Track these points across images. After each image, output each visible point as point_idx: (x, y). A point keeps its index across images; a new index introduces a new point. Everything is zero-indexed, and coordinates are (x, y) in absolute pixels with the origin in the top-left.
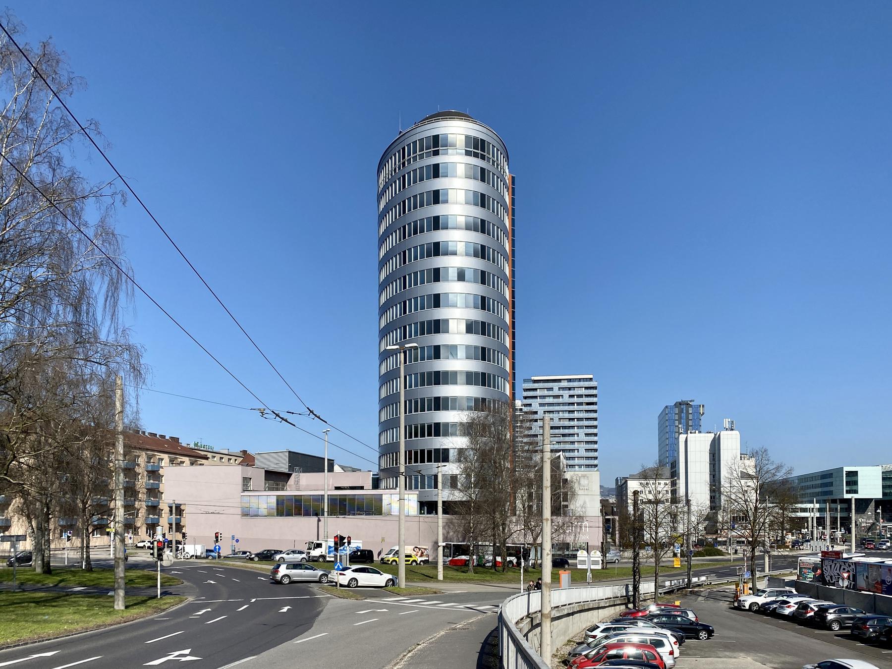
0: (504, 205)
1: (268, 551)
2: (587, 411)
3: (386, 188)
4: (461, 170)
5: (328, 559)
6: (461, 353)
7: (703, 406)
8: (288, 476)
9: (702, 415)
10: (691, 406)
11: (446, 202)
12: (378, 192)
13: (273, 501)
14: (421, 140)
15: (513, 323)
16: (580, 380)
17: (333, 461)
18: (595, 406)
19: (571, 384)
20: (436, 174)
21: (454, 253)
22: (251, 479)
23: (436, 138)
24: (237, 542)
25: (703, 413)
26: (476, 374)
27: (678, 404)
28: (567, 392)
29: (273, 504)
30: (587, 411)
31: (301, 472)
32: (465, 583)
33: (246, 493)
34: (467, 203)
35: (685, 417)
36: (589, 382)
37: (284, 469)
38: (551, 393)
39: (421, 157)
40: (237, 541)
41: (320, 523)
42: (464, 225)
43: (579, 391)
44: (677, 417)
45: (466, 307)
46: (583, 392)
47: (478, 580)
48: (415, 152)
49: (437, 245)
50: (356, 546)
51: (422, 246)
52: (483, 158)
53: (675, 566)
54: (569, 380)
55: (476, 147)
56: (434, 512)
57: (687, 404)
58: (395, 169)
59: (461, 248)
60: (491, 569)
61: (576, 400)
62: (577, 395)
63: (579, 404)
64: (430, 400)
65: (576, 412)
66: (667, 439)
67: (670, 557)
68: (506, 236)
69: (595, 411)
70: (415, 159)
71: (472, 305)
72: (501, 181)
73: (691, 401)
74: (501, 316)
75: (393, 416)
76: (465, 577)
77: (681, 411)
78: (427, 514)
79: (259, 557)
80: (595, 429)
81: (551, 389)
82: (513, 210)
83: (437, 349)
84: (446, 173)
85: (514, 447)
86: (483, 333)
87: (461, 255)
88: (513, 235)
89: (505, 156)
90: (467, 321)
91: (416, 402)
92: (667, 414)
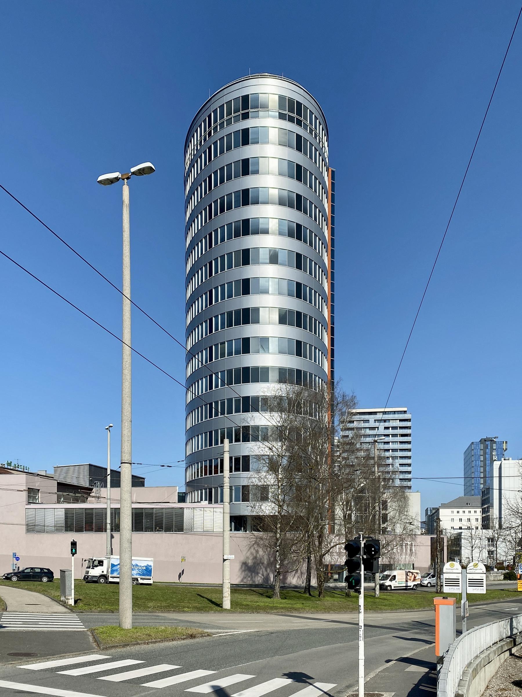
0: (322, 238)
1: (32, 568)
2: (401, 442)
3: (192, 166)
4: (273, 135)
5: (111, 580)
6: (273, 345)
7: (506, 442)
8: (89, 490)
9: (505, 451)
10: (495, 442)
11: (257, 172)
12: (185, 176)
13: (61, 514)
14: (229, 103)
15: (332, 372)
16: (394, 412)
17: (144, 479)
18: (409, 438)
19: (386, 417)
20: (246, 141)
21: (266, 232)
22: (39, 490)
23: (245, 98)
24: (17, 560)
25: (506, 449)
26: (291, 370)
27: (483, 441)
28: (382, 424)
29: (61, 517)
30: (401, 442)
31: (102, 487)
32: (263, 613)
33: (32, 506)
34: (280, 174)
35: (489, 453)
36: (403, 415)
37: (84, 482)
38: (367, 425)
39: (229, 122)
40: (18, 559)
41: (113, 540)
42: (277, 200)
43: (394, 423)
44: (482, 453)
45: (279, 294)
46: (398, 424)
47: (282, 608)
48: (222, 117)
49: (246, 222)
50: (146, 565)
51: (229, 225)
52: (299, 123)
53: (519, 590)
54: (385, 413)
55: (291, 110)
56: (242, 528)
57: (492, 441)
58: (201, 142)
59: (273, 225)
60: (305, 592)
61: (390, 431)
62: (391, 427)
63: (394, 435)
64: (238, 401)
65: (391, 443)
66: (473, 473)
67: (500, 580)
68: (324, 275)
69: (409, 443)
70: (222, 125)
71: (286, 292)
72: (319, 239)
73: (495, 438)
74: (319, 363)
75: (198, 421)
76: (267, 604)
77: (486, 447)
78: (235, 530)
79: (18, 577)
80: (409, 460)
81: (367, 421)
82: (332, 273)
83: (246, 342)
84: (256, 138)
85: (333, 456)
86: (299, 325)
87: (273, 234)
88: (333, 301)
89: (324, 128)
90: (280, 310)
91: (223, 404)
92: (473, 450)
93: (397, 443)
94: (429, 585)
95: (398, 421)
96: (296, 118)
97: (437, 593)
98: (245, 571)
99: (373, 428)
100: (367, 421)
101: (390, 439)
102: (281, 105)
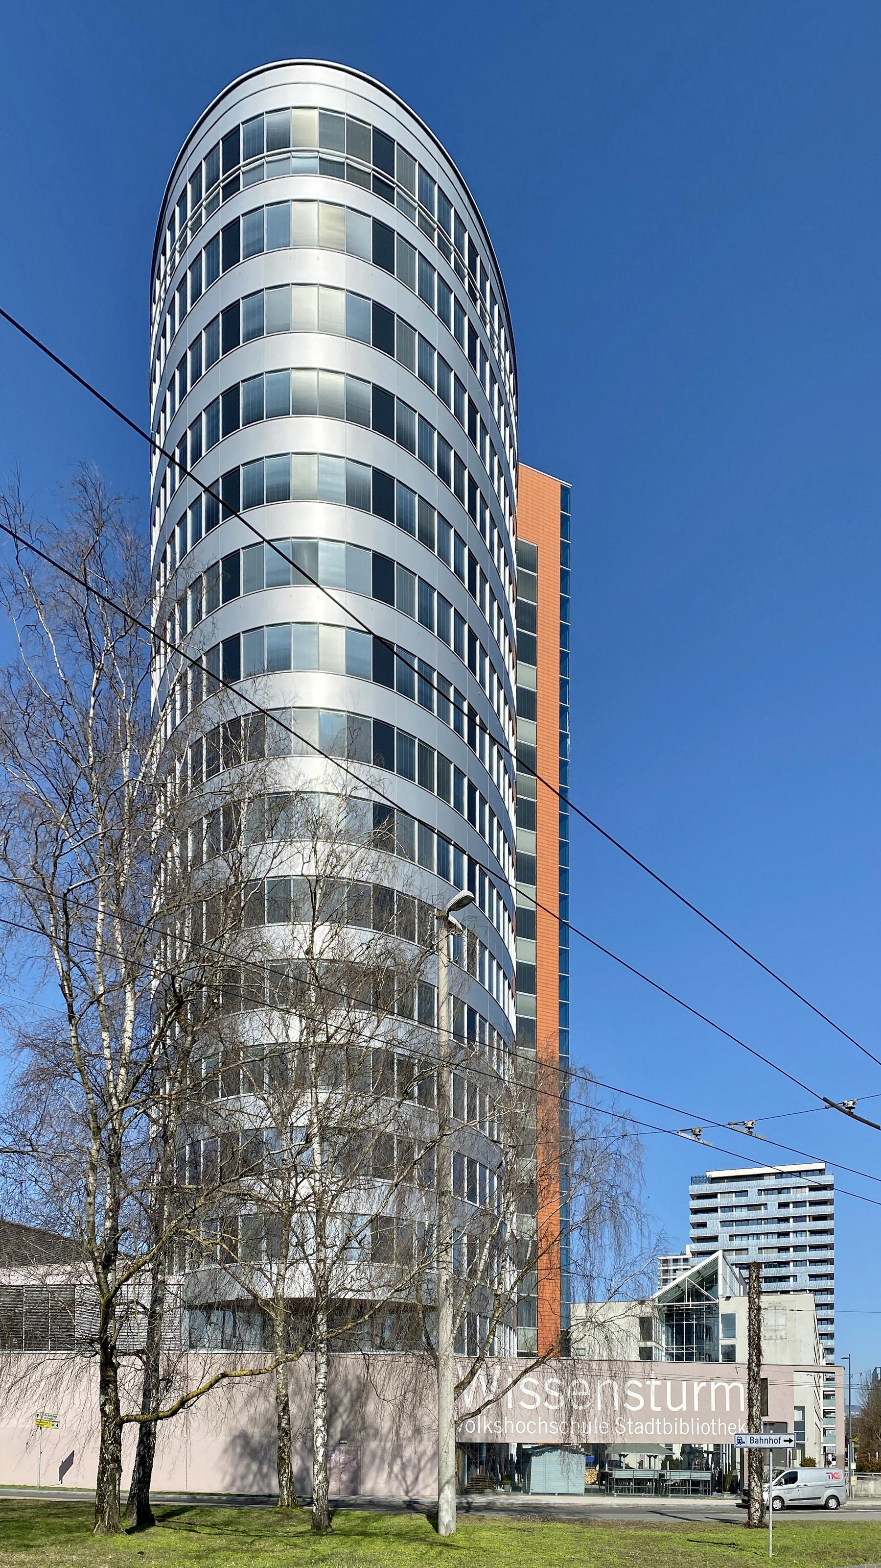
2: (813, 1232)
16: (799, 1173)
30: (813, 1232)
43: (799, 1195)
52: (384, 190)
54: (780, 1175)
61: (791, 1211)
62: (793, 1203)
65: (791, 1234)
81: (744, 1193)
93: (804, 1234)
94: (832, 1503)
95: (807, 1189)
96: (374, 175)
97: (748, 1525)
98: (241, 1456)
99: (756, 1207)
100: (744, 1193)
101: (791, 1225)
102: (326, 140)
